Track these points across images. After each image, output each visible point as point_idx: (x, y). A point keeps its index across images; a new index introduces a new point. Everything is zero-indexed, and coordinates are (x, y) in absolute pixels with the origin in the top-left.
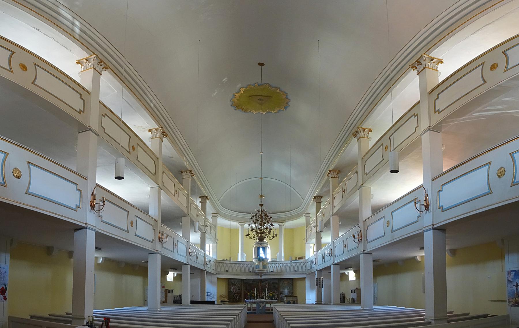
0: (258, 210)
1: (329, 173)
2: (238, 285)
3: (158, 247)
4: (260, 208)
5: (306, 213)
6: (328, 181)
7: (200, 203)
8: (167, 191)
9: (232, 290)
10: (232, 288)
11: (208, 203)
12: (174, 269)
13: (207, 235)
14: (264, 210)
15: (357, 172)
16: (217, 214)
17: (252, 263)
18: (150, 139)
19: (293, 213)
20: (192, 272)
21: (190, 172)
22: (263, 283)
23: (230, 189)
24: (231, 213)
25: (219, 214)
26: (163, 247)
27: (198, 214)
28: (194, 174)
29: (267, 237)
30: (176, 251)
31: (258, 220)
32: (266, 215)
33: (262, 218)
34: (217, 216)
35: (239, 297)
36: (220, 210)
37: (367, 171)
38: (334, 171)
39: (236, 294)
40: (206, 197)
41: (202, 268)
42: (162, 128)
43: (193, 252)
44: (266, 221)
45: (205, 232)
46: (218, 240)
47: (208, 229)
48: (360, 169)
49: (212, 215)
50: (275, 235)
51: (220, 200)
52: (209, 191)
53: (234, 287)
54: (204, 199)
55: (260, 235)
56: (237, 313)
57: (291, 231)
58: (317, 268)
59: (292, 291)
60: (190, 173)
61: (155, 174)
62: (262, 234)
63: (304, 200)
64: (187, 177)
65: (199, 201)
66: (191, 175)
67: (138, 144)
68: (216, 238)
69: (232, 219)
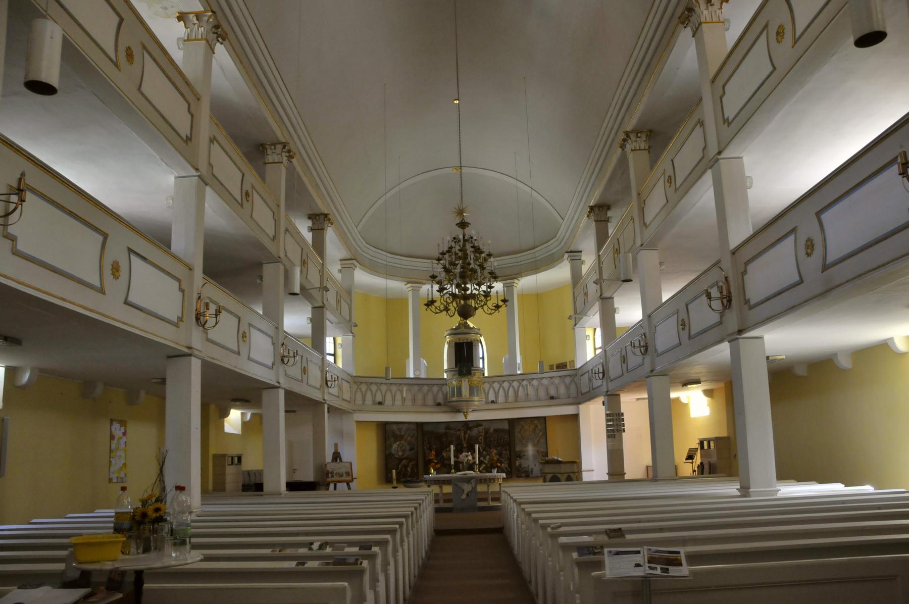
0: (454, 238)
1: (624, 140)
2: (409, 438)
3: (196, 339)
4: (459, 233)
5: (571, 252)
6: (623, 162)
7: (309, 232)
8: (222, 190)
9: (393, 452)
10: (395, 446)
11: (330, 234)
12: (242, 401)
13: (328, 315)
14: (472, 238)
15: (701, 123)
16: (350, 262)
17: (442, 383)
18: (181, 42)
19: (540, 253)
20: (289, 409)
21: (284, 147)
22: (470, 430)
23: (383, 199)
24: (389, 259)
25: (357, 261)
26: (209, 340)
27: (304, 257)
28: (295, 154)
29: (482, 306)
30: (244, 352)
31: (456, 265)
32: (477, 250)
33: (465, 257)
34: (352, 266)
35: (412, 469)
36: (360, 251)
37: (730, 113)
38: (637, 132)
39: (404, 462)
40: (326, 215)
41: (316, 395)
42: (212, 11)
43: (291, 354)
44: (476, 267)
45: (322, 304)
46: (356, 326)
47: (331, 297)
48: (708, 110)
49: (341, 265)
50: (502, 301)
51: (360, 227)
52: (333, 202)
53: (398, 443)
54: (319, 221)
55: (462, 302)
56: (407, 511)
57: (538, 297)
58: (607, 388)
59: (544, 450)
60: (284, 150)
61: (188, 139)
62: (469, 299)
63: (566, 219)
64: (276, 161)
65: (308, 227)
66: (287, 154)
67: (144, 47)
68: (350, 320)
69: (389, 272)
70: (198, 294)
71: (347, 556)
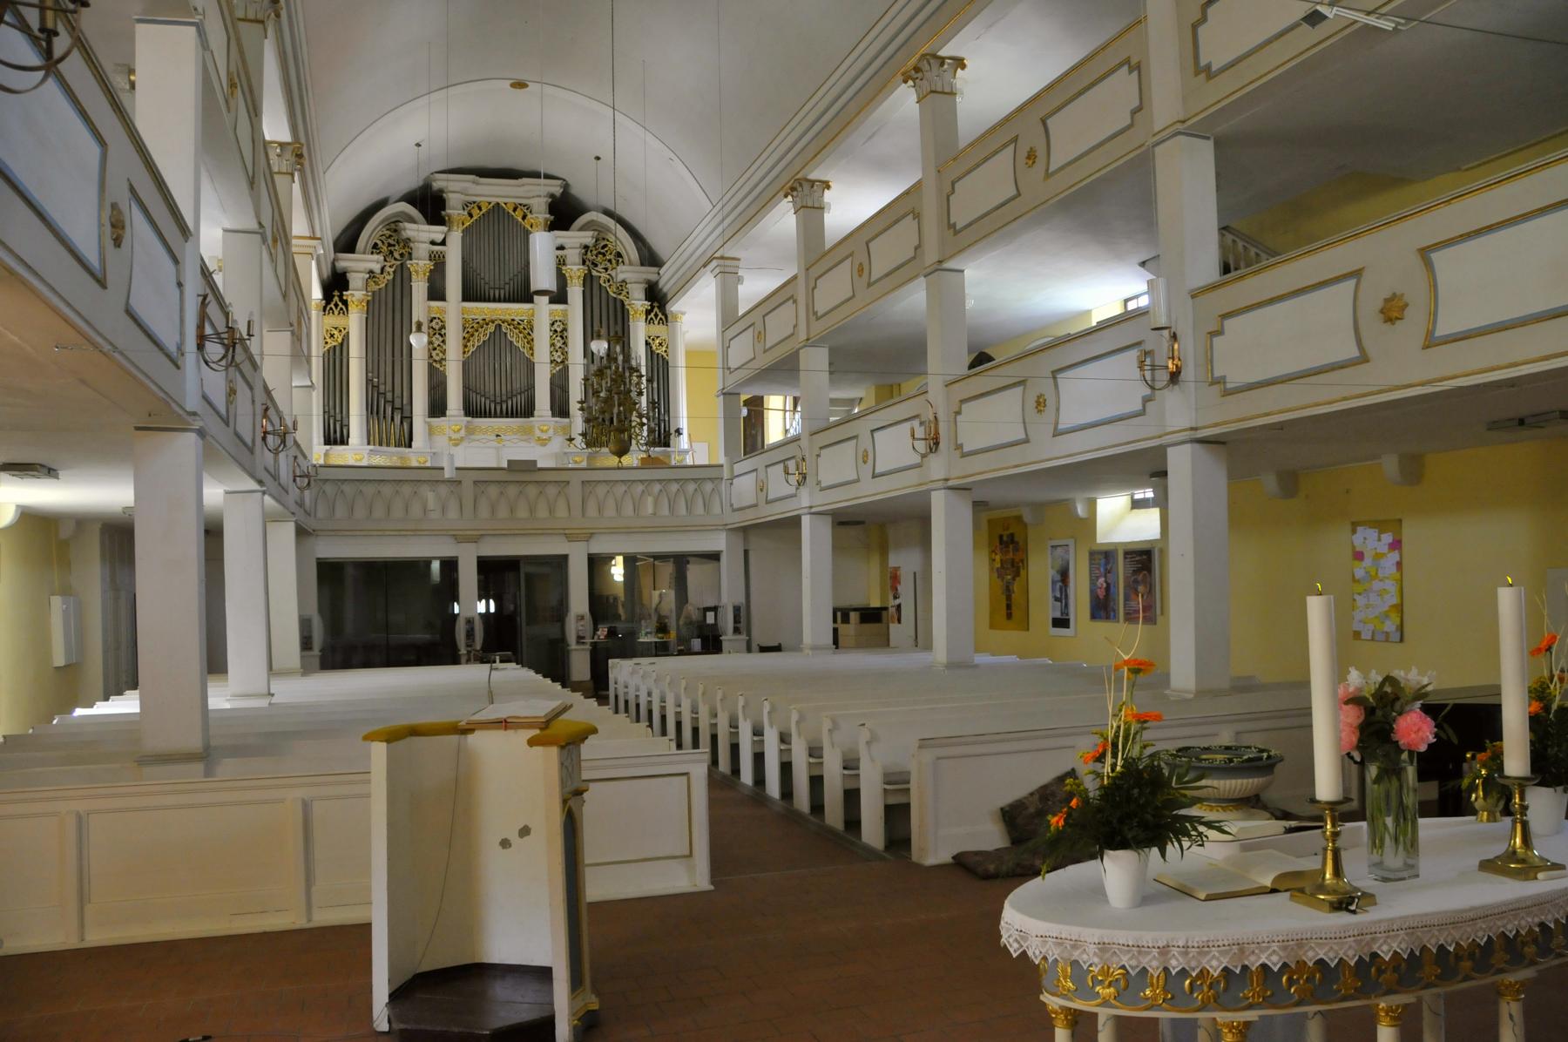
70: (263, 404)
71: (1154, 740)
